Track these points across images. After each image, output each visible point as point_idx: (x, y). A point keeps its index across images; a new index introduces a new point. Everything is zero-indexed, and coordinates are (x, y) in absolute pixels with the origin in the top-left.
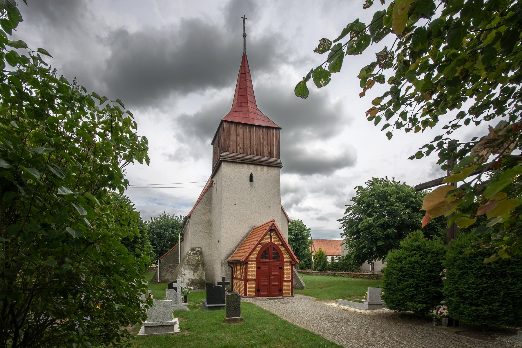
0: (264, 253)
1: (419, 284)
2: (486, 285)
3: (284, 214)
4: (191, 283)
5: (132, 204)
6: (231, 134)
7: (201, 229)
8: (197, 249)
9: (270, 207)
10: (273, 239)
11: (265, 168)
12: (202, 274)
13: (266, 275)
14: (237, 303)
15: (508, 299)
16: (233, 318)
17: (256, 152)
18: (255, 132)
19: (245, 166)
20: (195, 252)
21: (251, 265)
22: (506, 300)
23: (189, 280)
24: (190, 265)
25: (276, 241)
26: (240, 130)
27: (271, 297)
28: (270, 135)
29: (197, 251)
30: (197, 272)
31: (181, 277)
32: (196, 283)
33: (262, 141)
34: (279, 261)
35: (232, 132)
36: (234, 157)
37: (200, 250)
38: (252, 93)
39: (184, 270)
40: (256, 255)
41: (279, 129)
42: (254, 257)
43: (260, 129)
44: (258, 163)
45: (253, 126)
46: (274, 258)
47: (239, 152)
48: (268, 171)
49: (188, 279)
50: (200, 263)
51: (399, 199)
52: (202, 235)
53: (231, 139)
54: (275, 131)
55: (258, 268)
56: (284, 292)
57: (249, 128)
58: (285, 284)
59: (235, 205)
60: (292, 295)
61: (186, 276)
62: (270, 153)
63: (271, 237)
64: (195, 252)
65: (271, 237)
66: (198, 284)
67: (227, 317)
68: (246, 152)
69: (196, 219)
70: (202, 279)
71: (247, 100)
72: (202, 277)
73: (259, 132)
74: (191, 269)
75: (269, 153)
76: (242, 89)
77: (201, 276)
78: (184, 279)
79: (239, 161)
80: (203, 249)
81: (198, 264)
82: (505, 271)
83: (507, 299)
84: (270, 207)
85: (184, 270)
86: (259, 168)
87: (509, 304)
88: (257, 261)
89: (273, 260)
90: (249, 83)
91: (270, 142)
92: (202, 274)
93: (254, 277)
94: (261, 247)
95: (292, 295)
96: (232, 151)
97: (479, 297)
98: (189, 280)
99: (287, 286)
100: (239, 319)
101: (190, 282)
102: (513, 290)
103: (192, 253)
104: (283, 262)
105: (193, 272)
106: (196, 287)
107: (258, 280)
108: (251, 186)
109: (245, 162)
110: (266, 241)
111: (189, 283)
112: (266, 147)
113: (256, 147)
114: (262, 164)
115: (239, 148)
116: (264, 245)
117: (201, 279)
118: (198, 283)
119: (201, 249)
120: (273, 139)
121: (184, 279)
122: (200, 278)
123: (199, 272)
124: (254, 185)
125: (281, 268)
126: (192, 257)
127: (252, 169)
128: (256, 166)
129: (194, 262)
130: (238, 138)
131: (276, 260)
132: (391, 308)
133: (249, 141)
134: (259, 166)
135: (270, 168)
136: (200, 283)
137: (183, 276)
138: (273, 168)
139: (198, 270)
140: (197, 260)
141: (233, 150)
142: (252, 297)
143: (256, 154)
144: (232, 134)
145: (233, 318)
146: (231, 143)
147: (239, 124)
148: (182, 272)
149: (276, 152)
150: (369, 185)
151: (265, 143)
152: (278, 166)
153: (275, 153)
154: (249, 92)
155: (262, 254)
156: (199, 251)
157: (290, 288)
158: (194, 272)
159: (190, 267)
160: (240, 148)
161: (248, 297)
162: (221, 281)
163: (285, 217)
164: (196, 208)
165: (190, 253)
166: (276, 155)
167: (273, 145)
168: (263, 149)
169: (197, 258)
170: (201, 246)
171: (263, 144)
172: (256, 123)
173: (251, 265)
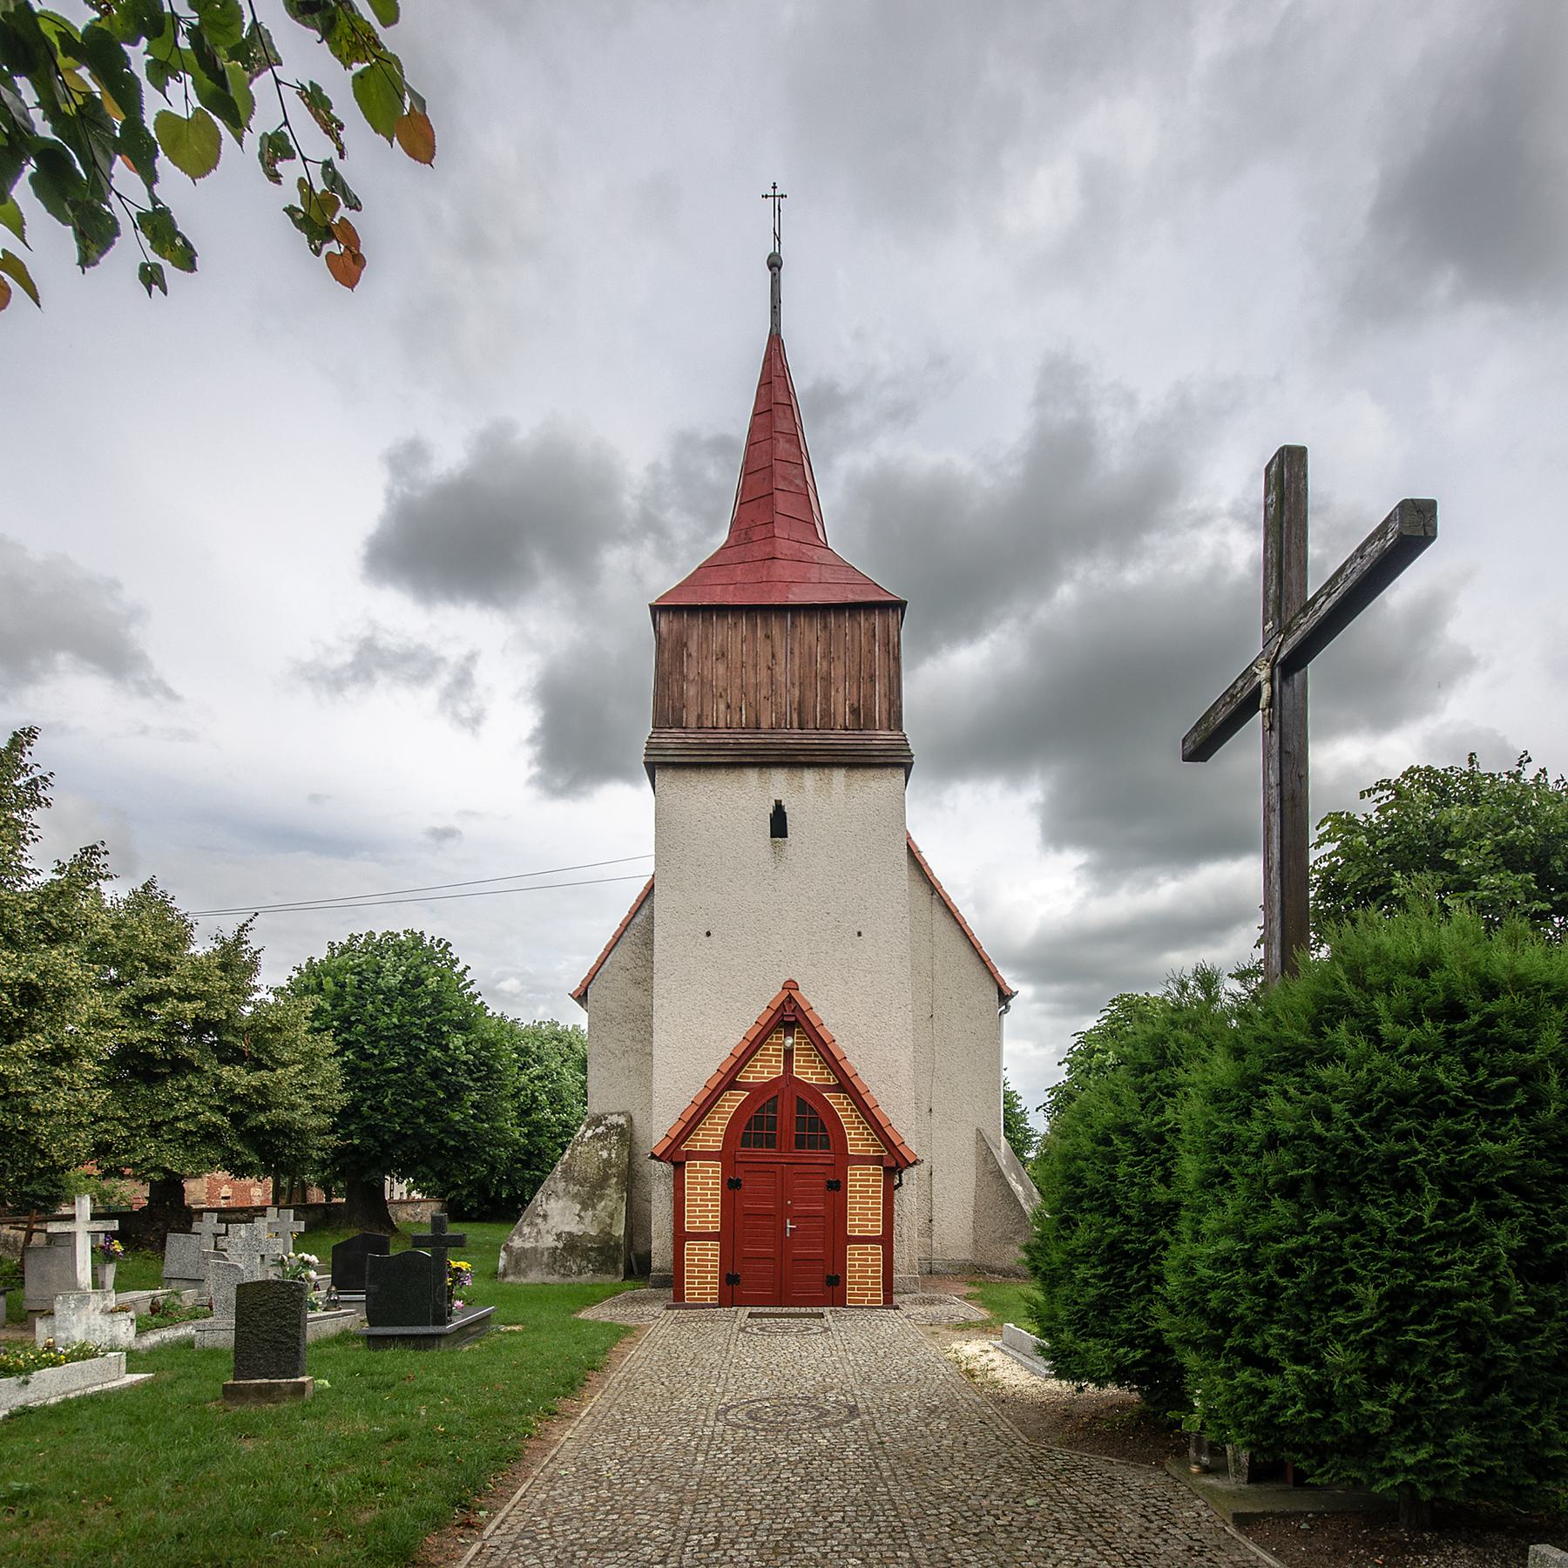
0: (756, 1121)
1: (1127, 1242)
2: (1293, 1243)
3: (981, 966)
4: (564, 1248)
5: (459, 968)
6: (689, 655)
7: (628, 1042)
8: (614, 1119)
9: (859, 934)
10: (798, 1062)
11: (839, 776)
12: (611, 1216)
13: (767, 1215)
14: (283, 1318)
15: (1427, 1335)
16: (258, 1381)
17: (795, 716)
18: (793, 638)
19: (752, 776)
20: (600, 1129)
21: (698, 1171)
22: (1411, 1337)
23: (559, 1236)
24: (573, 1178)
25: (809, 1073)
26: (725, 634)
27: (792, 1310)
28: (857, 638)
29: (610, 1128)
30: (594, 1208)
31: (531, 1224)
32: (583, 1250)
33: (822, 665)
34: (821, 1155)
35: (693, 647)
36: (701, 746)
37: (622, 1120)
38: (799, 482)
39: (547, 1199)
40: (721, 1130)
41: (899, 606)
42: (711, 1136)
43: (811, 626)
44: (803, 759)
45: (782, 610)
46: (800, 1143)
47: (722, 724)
48: (848, 786)
49: (554, 1231)
50: (614, 1170)
51: (1510, 857)
52: (632, 1063)
53: (691, 677)
54: (877, 620)
55: (731, 1185)
56: (852, 1290)
57: (766, 620)
58: (853, 1253)
59: (708, 934)
60: (888, 1302)
61: (551, 1222)
62: (855, 711)
63: (789, 1053)
64: (600, 1129)
65: (789, 1053)
66: (593, 1254)
67: (303, 1384)
68: (754, 719)
69: (611, 1005)
70: (609, 1233)
71: (774, 512)
72: (611, 1225)
73: (810, 631)
74: (575, 1196)
75: (851, 712)
76: (757, 475)
77: (608, 1221)
78: (539, 1232)
79: (721, 760)
80: (636, 1121)
81: (606, 1178)
82: (1406, 1154)
83: (1419, 1334)
84: (859, 934)
85: (547, 1199)
86: (810, 778)
87: (1439, 1365)
88: (724, 1156)
89: (797, 1152)
90: (787, 446)
91: (857, 668)
92: (611, 1216)
93: (713, 1223)
94: (742, 1096)
95: (888, 1302)
96: (693, 722)
97: (1267, 1315)
98: (559, 1236)
99: (861, 1263)
100: (289, 1389)
101: (560, 1245)
102: (1448, 1278)
103: (590, 1133)
104: (845, 1159)
105: (579, 1207)
106: (584, 1263)
107: (728, 1236)
108: (777, 853)
109: (748, 760)
110: (766, 1070)
111: (557, 1248)
112: (841, 690)
113: (797, 693)
114: (818, 759)
115: (722, 707)
116: (757, 1091)
117: (606, 1234)
118: (592, 1249)
119: (630, 1120)
120: (871, 651)
121: (539, 1232)
122: (602, 1231)
123: (605, 1207)
124: (789, 851)
125: (837, 1186)
126: (586, 1149)
127: (779, 785)
128: (798, 773)
129: (592, 1171)
130: (721, 669)
131: (807, 1152)
132: (1063, 1363)
133: (764, 675)
134: (811, 771)
135: (859, 776)
136: (600, 1250)
137: (539, 1221)
138: (871, 773)
139: (601, 1197)
140: (604, 1160)
141: (699, 717)
142: (709, 1306)
143: (795, 725)
144: (694, 654)
145: (258, 1381)
146: (691, 691)
147: (722, 610)
148: (536, 1208)
149: (885, 706)
150: (1384, 801)
151: (838, 671)
152: (898, 761)
153: (880, 708)
154: (784, 478)
155: (748, 1127)
156: (618, 1126)
157: (851, 1266)
158: (584, 1208)
159: (571, 1187)
160: (728, 707)
161: (686, 1307)
162: (427, 1232)
163: (988, 977)
164: (607, 962)
165: (582, 1136)
166: (884, 715)
167: (872, 678)
168: (827, 697)
169: (605, 1154)
170: (630, 1108)
171: (827, 679)
172: (797, 596)
173: (698, 1171)
